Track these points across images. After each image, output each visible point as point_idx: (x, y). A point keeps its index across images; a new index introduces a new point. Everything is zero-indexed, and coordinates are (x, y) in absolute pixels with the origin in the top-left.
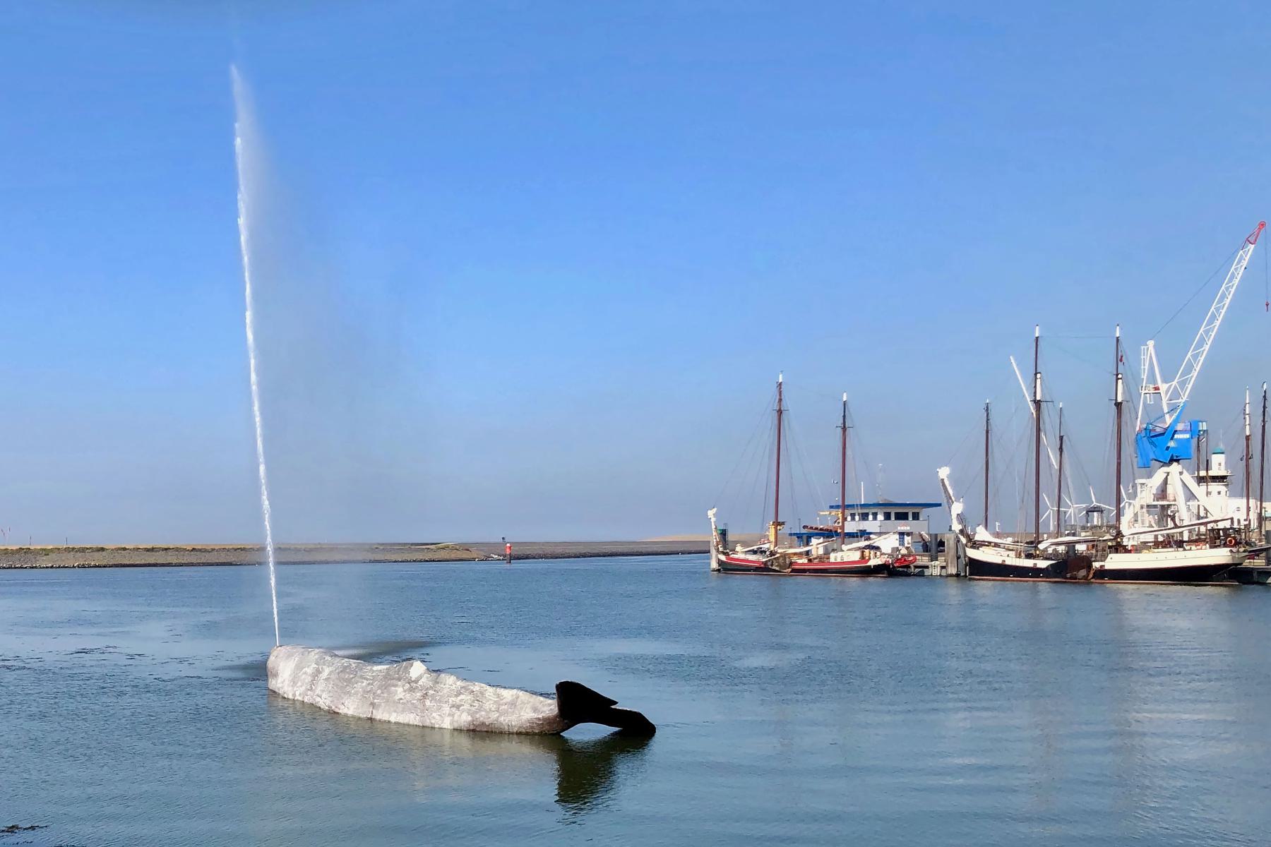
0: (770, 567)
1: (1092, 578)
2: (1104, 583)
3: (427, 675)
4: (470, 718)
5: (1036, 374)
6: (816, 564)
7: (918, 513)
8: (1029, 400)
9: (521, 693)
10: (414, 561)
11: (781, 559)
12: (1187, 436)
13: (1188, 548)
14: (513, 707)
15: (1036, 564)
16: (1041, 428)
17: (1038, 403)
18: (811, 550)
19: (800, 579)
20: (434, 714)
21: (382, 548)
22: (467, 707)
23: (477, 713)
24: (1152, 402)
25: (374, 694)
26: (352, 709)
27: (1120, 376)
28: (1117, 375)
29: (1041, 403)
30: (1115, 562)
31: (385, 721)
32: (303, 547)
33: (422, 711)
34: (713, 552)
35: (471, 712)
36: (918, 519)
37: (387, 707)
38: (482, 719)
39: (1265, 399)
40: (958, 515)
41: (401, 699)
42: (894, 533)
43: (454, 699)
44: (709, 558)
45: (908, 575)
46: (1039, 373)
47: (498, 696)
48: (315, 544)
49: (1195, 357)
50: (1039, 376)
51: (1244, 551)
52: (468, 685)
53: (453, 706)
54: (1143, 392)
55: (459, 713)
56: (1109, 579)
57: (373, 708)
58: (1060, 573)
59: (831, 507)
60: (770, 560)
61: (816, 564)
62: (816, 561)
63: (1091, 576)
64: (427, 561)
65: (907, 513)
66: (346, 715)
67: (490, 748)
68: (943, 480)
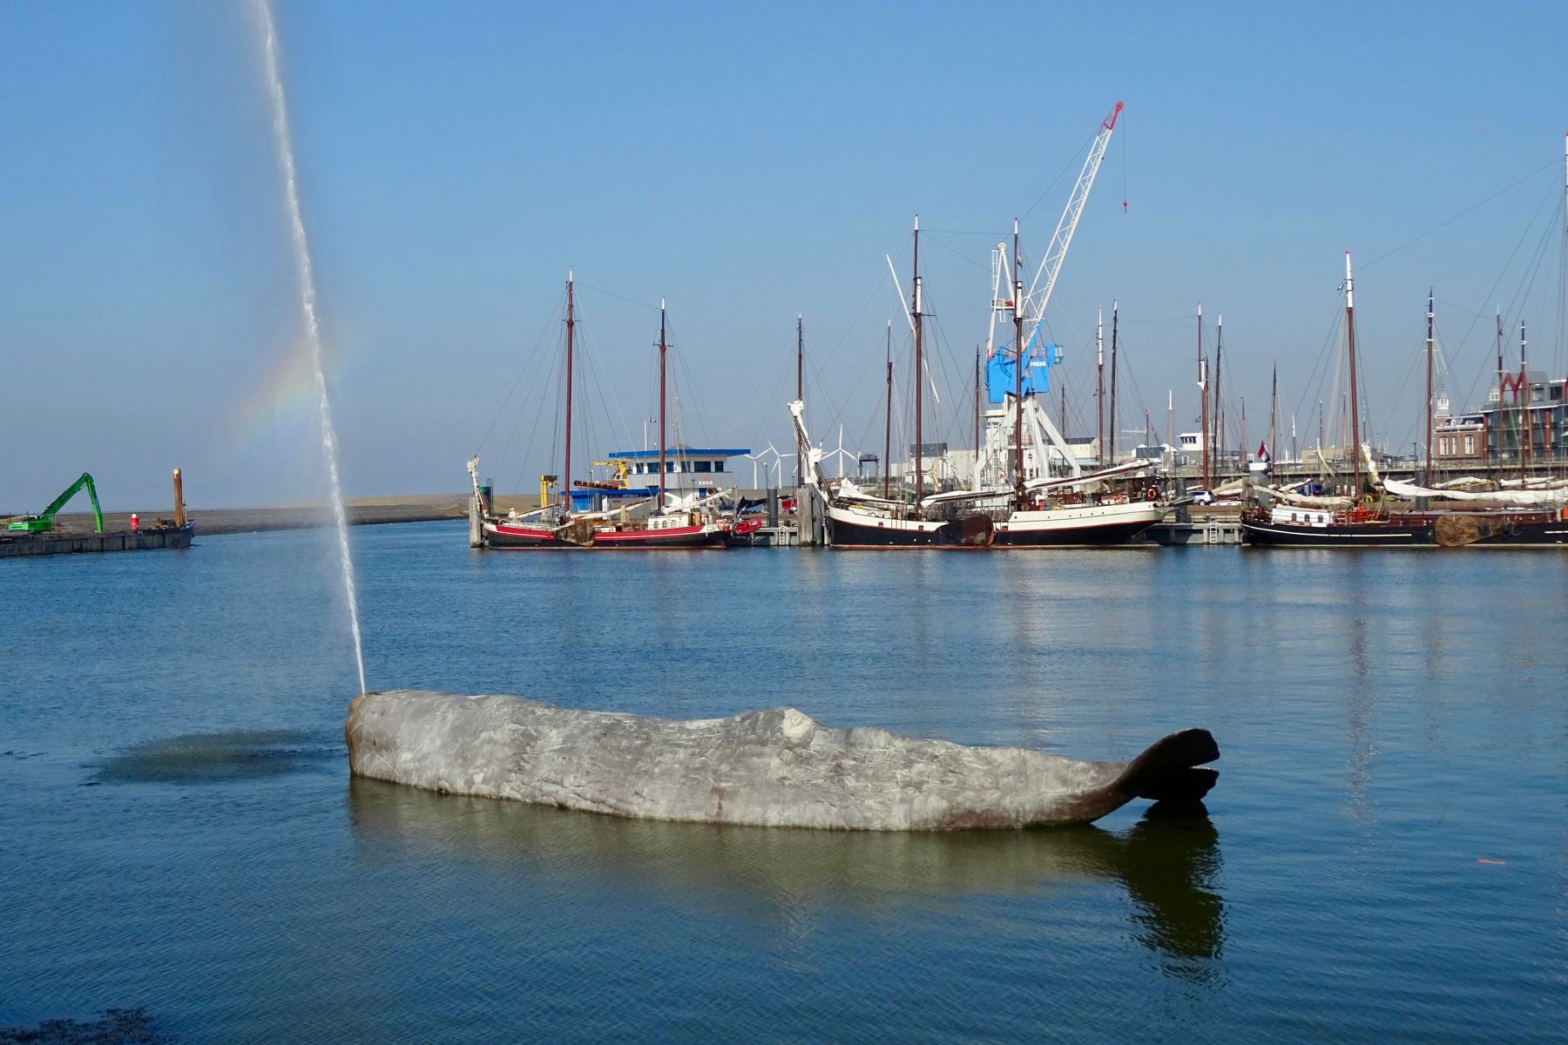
0: (563, 539)
3: (819, 733)
4: (944, 804)
5: (915, 279)
6: (626, 534)
7: (722, 463)
9: (1027, 754)
13: (1105, 502)
15: (922, 527)
16: (923, 351)
17: (917, 316)
19: (611, 556)
20: (870, 802)
22: (934, 783)
23: (957, 794)
24: (1005, 321)
25: (715, 772)
26: (663, 802)
27: (1019, 285)
28: (1016, 283)
30: (1022, 521)
33: (842, 798)
34: (474, 519)
35: (945, 793)
38: (968, 804)
40: (816, 463)
41: (785, 778)
42: (694, 490)
43: (905, 772)
44: (468, 529)
46: (920, 278)
47: (988, 761)
49: (1050, 265)
50: (919, 281)
51: (1170, 505)
52: (920, 746)
53: (907, 785)
54: (995, 307)
55: (921, 797)
56: (1014, 544)
57: (721, 798)
58: (952, 537)
59: (612, 455)
60: (563, 529)
61: (626, 534)
62: (625, 530)
63: (991, 540)
66: (650, 821)
68: (796, 417)
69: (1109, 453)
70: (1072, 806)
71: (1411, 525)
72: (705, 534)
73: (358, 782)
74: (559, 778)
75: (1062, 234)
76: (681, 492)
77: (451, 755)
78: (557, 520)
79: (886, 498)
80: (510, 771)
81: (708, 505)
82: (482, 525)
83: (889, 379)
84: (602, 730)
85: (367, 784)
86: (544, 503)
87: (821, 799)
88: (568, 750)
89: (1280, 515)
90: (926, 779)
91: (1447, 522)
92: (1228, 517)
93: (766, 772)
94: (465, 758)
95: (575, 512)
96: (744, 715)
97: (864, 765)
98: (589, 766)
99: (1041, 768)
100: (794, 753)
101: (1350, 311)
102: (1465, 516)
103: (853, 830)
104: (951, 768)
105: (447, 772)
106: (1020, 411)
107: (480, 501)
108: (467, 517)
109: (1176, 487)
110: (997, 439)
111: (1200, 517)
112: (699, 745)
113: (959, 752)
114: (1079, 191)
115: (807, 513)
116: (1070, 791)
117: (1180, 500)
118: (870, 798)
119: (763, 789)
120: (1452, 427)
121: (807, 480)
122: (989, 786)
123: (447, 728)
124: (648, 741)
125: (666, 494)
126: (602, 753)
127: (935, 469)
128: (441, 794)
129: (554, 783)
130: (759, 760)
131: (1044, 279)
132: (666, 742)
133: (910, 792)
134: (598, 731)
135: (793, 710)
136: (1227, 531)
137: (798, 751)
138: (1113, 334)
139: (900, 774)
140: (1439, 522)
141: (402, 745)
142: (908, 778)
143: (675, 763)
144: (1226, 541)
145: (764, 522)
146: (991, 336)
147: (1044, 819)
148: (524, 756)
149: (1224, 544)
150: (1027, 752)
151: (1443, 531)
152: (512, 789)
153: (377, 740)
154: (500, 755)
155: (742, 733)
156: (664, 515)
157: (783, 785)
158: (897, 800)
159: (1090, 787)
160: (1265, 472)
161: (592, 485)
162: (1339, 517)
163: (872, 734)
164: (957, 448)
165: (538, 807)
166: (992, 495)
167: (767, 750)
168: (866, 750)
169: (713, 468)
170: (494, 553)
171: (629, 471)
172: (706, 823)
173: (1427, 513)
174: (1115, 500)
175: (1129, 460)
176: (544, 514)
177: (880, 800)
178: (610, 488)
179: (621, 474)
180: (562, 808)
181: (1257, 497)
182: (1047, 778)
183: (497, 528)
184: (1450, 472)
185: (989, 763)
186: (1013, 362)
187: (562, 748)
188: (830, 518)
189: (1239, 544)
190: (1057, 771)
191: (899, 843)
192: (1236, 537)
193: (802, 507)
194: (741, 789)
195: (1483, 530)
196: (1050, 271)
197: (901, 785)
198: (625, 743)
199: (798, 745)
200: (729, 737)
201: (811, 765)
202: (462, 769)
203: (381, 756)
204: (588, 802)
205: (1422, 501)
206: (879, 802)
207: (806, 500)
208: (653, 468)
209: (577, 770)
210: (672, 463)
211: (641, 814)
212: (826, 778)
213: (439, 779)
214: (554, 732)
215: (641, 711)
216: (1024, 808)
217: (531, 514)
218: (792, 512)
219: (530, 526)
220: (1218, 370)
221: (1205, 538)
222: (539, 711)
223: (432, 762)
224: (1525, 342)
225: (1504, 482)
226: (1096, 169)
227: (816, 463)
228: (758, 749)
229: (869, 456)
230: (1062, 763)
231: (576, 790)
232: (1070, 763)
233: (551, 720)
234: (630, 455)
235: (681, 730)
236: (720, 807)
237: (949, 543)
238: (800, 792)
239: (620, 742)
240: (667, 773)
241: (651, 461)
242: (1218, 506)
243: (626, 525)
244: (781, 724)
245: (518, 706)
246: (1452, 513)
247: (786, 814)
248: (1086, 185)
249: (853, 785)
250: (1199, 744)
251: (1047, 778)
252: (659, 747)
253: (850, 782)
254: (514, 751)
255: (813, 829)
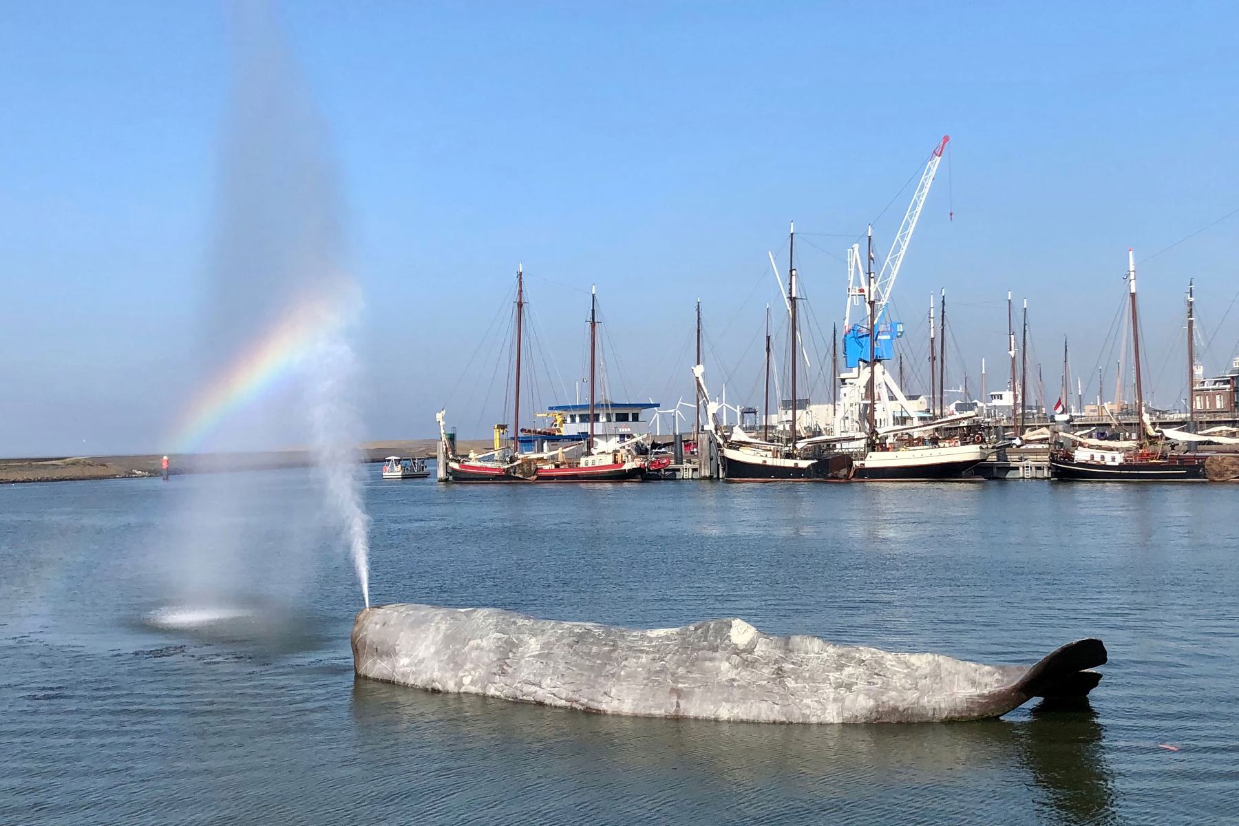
0: (513, 474)
1: (853, 477)
2: (864, 482)
4: (871, 703)
5: (791, 271)
7: (638, 414)
8: (785, 297)
9: (941, 659)
10: (40, 481)
11: (525, 465)
13: (941, 445)
14: (938, 681)
18: (558, 454)
22: (862, 685)
23: (883, 694)
24: (858, 304)
25: (673, 674)
27: (872, 275)
28: (870, 273)
29: (796, 301)
30: (876, 460)
31: (707, 720)
34: (441, 459)
36: (637, 420)
39: (944, 304)
40: (714, 414)
41: (734, 680)
42: (615, 435)
43: (837, 674)
45: (659, 478)
46: (795, 270)
47: (908, 665)
50: (794, 272)
51: (993, 448)
52: (849, 652)
54: (851, 293)
55: (852, 696)
56: (870, 478)
57: (678, 698)
59: (551, 408)
60: (512, 467)
62: (562, 467)
64: (55, 480)
65: (628, 414)
66: (617, 716)
68: (697, 378)
70: (982, 705)
72: (625, 470)
73: (361, 682)
74: (537, 680)
75: (902, 237)
76: (606, 437)
77: (442, 661)
78: (508, 459)
79: (766, 440)
80: (495, 674)
81: (627, 448)
82: (447, 464)
84: (575, 638)
85: (370, 686)
86: (497, 445)
88: (545, 656)
89: (1081, 455)
90: (855, 681)
91: (1214, 462)
92: (1038, 457)
93: (717, 674)
94: (456, 663)
96: (696, 625)
97: (801, 669)
98: (564, 670)
100: (741, 657)
101: (1133, 296)
102: (1228, 456)
104: (876, 671)
105: (440, 675)
106: (872, 372)
107: (446, 445)
108: (435, 457)
109: (997, 433)
110: (852, 395)
114: (916, 204)
115: (706, 453)
117: (1000, 443)
119: (715, 690)
120: (1205, 387)
121: (706, 428)
122: (910, 687)
123: (440, 636)
125: (595, 439)
126: (575, 658)
127: (804, 419)
128: (435, 691)
129: (534, 684)
130: (711, 664)
132: (630, 648)
133: (842, 692)
134: (571, 639)
135: (739, 620)
136: (1038, 468)
137: (744, 655)
138: (941, 314)
139: (832, 676)
140: (1207, 461)
141: (401, 651)
142: (840, 680)
143: (638, 667)
144: (1038, 476)
145: (672, 461)
147: (957, 715)
148: (507, 661)
149: (1036, 478)
150: (941, 657)
151: (1212, 469)
152: (496, 689)
153: (379, 648)
154: (486, 660)
155: (696, 640)
156: (593, 455)
157: (732, 686)
158: (831, 699)
159: (995, 688)
161: (535, 432)
162: (1128, 457)
163: (807, 641)
165: (517, 703)
166: (853, 439)
167: (717, 655)
168: (802, 655)
169: (630, 418)
171: (564, 421)
172: (666, 718)
173: (1197, 454)
174: (949, 443)
175: (951, 412)
176: (496, 455)
177: (816, 699)
178: (550, 434)
179: (558, 423)
180: (540, 704)
181: (1061, 441)
182: (958, 680)
183: (461, 466)
184: (1207, 422)
186: (867, 335)
187: (539, 654)
188: (724, 457)
189: (1048, 478)
190: (967, 674)
192: (1046, 473)
193: (702, 449)
196: (894, 266)
197: (834, 686)
198: (594, 649)
199: (744, 651)
200: (685, 645)
202: (453, 673)
203: (383, 661)
205: (1193, 445)
206: (816, 701)
207: (706, 443)
208: (584, 419)
210: (598, 415)
211: (610, 711)
212: (769, 680)
214: (533, 640)
215: (609, 623)
216: (939, 705)
217: (487, 455)
218: (693, 453)
219: (486, 465)
220: (1024, 342)
221: (1021, 473)
222: (520, 622)
223: (426, 667)
226: (928, 186)
227: (714, 414)
228: (710, 654)
229: (749, 409)
233: (531, 630)
234: (566, 408)
235: (643, 637)
236: (678, 706)
238: (747, 693)
239: (591, 649)
240: (631, 676)
243: (563, 463)
244: (729, 632)
246: (1217, 454)
247: (735, 711)
248: (921, 198)
249: (792, 686)
250: (1093, 651)
251: (958, 680)
252: (624, 653)
253: (791, 683)
254: (499, 656)
255: (759, 723)
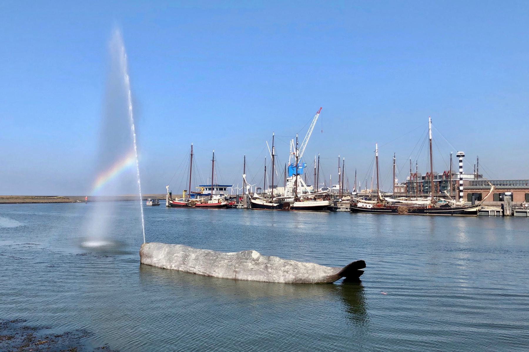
3: (261, 257)
4: (294, 277)
5: (273, 147)
7: (226, 188)
8: (271, 155)
10: (49, 203)
12: (302, 168)
13: (317, 200)
14: (314, 271)
17: (273, 156)
20: (274, 276)
21: (36, 198)
22: (291, 271)
23: (297, 274)
25: (234, 266)
27: (297, 149)
28: (297, 148)
30: (297, 204)
32: (5, 197)
33: (268, 274)
34: (167, 200)
37: (245, 273)
38: (300, 277)
41: (253, 269)
42: (219, 194)
43: (284, 268)
44: (166, 202)
48: (10, 196)
50: (274, 147)
51: (333, 202)
52: (287, 261)
53: (284, 271)
54: (291, 154)
55: (288, 275)
56: (295, 210)
57: (236, 273)
58: (280, 208)
59: (200, 186)
62: (203, 203)
63: (289, 208)
64: (54, 203)
66: (218, 278)
67: (303, 293)
69: (317, 189)
71: (392, 208)
73: (142, 265)
75: (307, 138)
76: (216, 195)
78: (187, 201)
80: (181, 264)
81: (222, 198)
82: (169, 201)
83: (265, 170)
87: (262, 274)
88: (197, 259)
89: (360, 205)
94: (170, 260)
95: (191, 199)
96: (242, 252)
99: (319, 268)
101: (377, 157)
103: (269, 282)
104: (296, 268)
105: (165, 264)
106: (297, 178)
108: (166, 199)
109: (334, 197)
110: (290, 185)
111: (340, 205)
112: (230, 259)
113: (297, 263)
115: (246, 201)
116: (326, 275)
117: (335, 200)
118: (275, 275)
121: (246, 193)
124: (217, 257)
127: (275, 191)
129: (193, 268)
130: (246, 264)
131: (302, 148)
132: (222, 258)
136: (346, 208)
137: (256, 261)
139: (282, 269)
140: (398, 208)
143: (224, 264)
146: (290, 160)
147: (320, 282)
149: (346, 211)
150: (315, 264)
152: (182, 269)
157: (252, 270)
160: (356, 195)
161: (195, 193)
164: (279, 187)
165: (188, 273)
166: (290, 198)
167: (248, 261)
169: (223, 190)
170: (172, 208)
171: (204, 190)
172: (232, 279)
175: (320, 191)
178: (199, 193)
180: (195, 274)
184: (399, 196)
185: (305, 267)
186: (295, 167)
189: (349, 211)
191: (282, 286)
192: (349, 210)
193: (245, 199)
194: (241, 271)
195: (409, 210)
196: (304, 146)
198: (211, 258)
199: (255, 260)
200: (238, 258)
201: (259, 265)
203: (149, 259)
204: (202, 273)
209: (199, 265)
210: (214, 188)
211: (215, 276)
212: (263, 269)
213: (163, 266)
214: (193, 254)
215: (215, 249)
216: (314, 279)
218: (242, 200)
220: (343, 170)
222: (189, 249)
224: (417, 166)
225: (412, 199)
228: (245, 260)
230: (324, 267)
231: (199, 269)
232: (326, 267)
233: (193, 251)
234: (204, 186)
236: (236, 275)
237: (279, 209)
238: (257, 272)
239: (210, 258)
240: (222, 266)
241: (209, 187)
242: (343, 202)
243: (203, 202)
245: (184, 247)
251: (320, 271)
255: (260, 282)
